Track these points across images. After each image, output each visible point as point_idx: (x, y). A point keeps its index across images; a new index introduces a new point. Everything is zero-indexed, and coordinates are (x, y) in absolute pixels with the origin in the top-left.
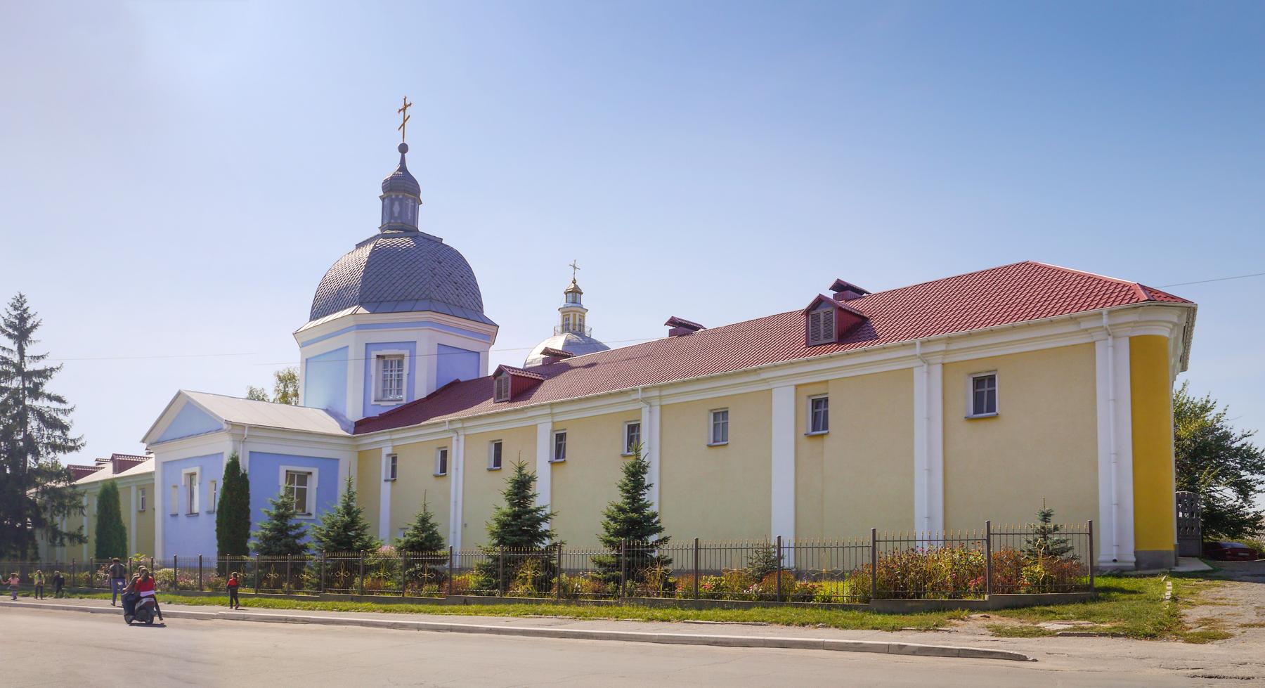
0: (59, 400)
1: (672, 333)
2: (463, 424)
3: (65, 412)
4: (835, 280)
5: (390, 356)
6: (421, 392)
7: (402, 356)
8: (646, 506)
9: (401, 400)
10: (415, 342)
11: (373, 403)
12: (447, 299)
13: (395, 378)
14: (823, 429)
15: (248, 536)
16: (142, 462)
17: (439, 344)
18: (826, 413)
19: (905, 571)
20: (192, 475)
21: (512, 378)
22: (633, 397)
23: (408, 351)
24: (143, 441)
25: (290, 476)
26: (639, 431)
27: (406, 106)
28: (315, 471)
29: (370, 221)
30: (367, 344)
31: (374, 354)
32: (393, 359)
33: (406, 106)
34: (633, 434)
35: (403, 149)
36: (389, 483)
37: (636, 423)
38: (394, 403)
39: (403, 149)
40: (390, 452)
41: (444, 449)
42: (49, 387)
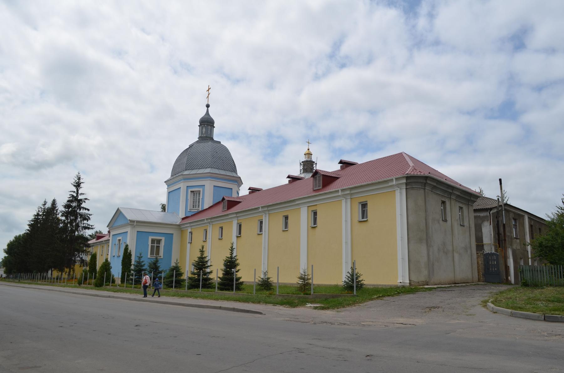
0: (88, 210)
1: (250, 193)
2: (190, 224)
3: (90, 215)
4: (249, 187)
5: (196, 191)
6: (206, 207)
7: (200, 191)
8: (205, 257)
9: (199, 209)
10: (205, 185)
11: (189, 210)
12: (219, 167)
13: (197, 200)
14: (366, 218)
15: (489, 253)
16: (105, 236)
17: (214, 186)
18: (367, 210)
19: (81, 276)
20: (120, 240)
21: (228, 202)
22: (390, 184)
23: (202, 189)
24: (107, 227)
25: (153, 241)
26: (367, 208)
27: (209, 89)
28: (163, 239)
29: (193, 136)
30: (187, 186)
31: (190, 190)
32: (197, 192)
33: (209, 89)
34: (364, 209)
35: (208, 106)
36: (190, 244)
37: (365, 203)
38: (196, 211)
39: (208, 106)
40: (190, 231)
41: (240, 224)
42: (83, 205)
